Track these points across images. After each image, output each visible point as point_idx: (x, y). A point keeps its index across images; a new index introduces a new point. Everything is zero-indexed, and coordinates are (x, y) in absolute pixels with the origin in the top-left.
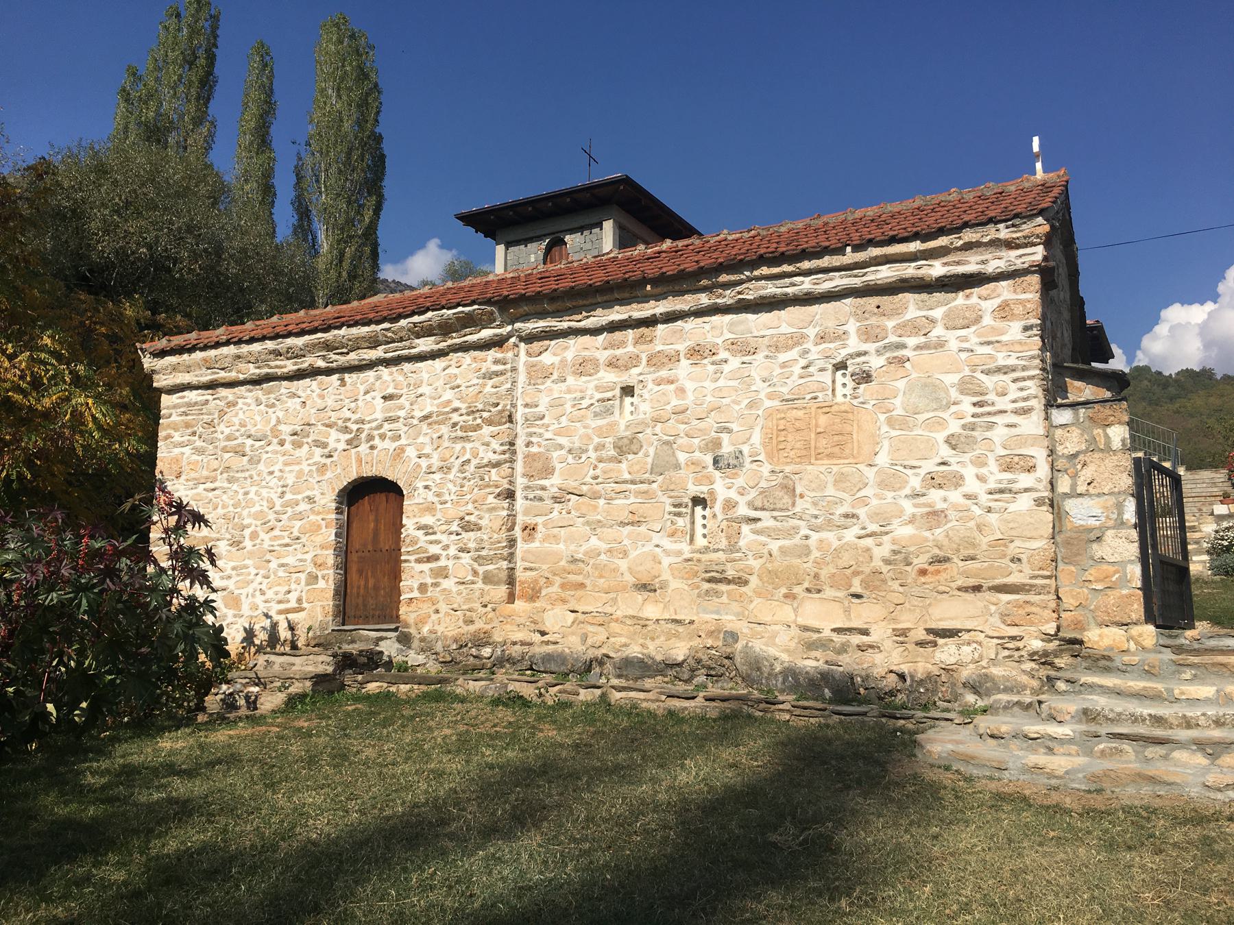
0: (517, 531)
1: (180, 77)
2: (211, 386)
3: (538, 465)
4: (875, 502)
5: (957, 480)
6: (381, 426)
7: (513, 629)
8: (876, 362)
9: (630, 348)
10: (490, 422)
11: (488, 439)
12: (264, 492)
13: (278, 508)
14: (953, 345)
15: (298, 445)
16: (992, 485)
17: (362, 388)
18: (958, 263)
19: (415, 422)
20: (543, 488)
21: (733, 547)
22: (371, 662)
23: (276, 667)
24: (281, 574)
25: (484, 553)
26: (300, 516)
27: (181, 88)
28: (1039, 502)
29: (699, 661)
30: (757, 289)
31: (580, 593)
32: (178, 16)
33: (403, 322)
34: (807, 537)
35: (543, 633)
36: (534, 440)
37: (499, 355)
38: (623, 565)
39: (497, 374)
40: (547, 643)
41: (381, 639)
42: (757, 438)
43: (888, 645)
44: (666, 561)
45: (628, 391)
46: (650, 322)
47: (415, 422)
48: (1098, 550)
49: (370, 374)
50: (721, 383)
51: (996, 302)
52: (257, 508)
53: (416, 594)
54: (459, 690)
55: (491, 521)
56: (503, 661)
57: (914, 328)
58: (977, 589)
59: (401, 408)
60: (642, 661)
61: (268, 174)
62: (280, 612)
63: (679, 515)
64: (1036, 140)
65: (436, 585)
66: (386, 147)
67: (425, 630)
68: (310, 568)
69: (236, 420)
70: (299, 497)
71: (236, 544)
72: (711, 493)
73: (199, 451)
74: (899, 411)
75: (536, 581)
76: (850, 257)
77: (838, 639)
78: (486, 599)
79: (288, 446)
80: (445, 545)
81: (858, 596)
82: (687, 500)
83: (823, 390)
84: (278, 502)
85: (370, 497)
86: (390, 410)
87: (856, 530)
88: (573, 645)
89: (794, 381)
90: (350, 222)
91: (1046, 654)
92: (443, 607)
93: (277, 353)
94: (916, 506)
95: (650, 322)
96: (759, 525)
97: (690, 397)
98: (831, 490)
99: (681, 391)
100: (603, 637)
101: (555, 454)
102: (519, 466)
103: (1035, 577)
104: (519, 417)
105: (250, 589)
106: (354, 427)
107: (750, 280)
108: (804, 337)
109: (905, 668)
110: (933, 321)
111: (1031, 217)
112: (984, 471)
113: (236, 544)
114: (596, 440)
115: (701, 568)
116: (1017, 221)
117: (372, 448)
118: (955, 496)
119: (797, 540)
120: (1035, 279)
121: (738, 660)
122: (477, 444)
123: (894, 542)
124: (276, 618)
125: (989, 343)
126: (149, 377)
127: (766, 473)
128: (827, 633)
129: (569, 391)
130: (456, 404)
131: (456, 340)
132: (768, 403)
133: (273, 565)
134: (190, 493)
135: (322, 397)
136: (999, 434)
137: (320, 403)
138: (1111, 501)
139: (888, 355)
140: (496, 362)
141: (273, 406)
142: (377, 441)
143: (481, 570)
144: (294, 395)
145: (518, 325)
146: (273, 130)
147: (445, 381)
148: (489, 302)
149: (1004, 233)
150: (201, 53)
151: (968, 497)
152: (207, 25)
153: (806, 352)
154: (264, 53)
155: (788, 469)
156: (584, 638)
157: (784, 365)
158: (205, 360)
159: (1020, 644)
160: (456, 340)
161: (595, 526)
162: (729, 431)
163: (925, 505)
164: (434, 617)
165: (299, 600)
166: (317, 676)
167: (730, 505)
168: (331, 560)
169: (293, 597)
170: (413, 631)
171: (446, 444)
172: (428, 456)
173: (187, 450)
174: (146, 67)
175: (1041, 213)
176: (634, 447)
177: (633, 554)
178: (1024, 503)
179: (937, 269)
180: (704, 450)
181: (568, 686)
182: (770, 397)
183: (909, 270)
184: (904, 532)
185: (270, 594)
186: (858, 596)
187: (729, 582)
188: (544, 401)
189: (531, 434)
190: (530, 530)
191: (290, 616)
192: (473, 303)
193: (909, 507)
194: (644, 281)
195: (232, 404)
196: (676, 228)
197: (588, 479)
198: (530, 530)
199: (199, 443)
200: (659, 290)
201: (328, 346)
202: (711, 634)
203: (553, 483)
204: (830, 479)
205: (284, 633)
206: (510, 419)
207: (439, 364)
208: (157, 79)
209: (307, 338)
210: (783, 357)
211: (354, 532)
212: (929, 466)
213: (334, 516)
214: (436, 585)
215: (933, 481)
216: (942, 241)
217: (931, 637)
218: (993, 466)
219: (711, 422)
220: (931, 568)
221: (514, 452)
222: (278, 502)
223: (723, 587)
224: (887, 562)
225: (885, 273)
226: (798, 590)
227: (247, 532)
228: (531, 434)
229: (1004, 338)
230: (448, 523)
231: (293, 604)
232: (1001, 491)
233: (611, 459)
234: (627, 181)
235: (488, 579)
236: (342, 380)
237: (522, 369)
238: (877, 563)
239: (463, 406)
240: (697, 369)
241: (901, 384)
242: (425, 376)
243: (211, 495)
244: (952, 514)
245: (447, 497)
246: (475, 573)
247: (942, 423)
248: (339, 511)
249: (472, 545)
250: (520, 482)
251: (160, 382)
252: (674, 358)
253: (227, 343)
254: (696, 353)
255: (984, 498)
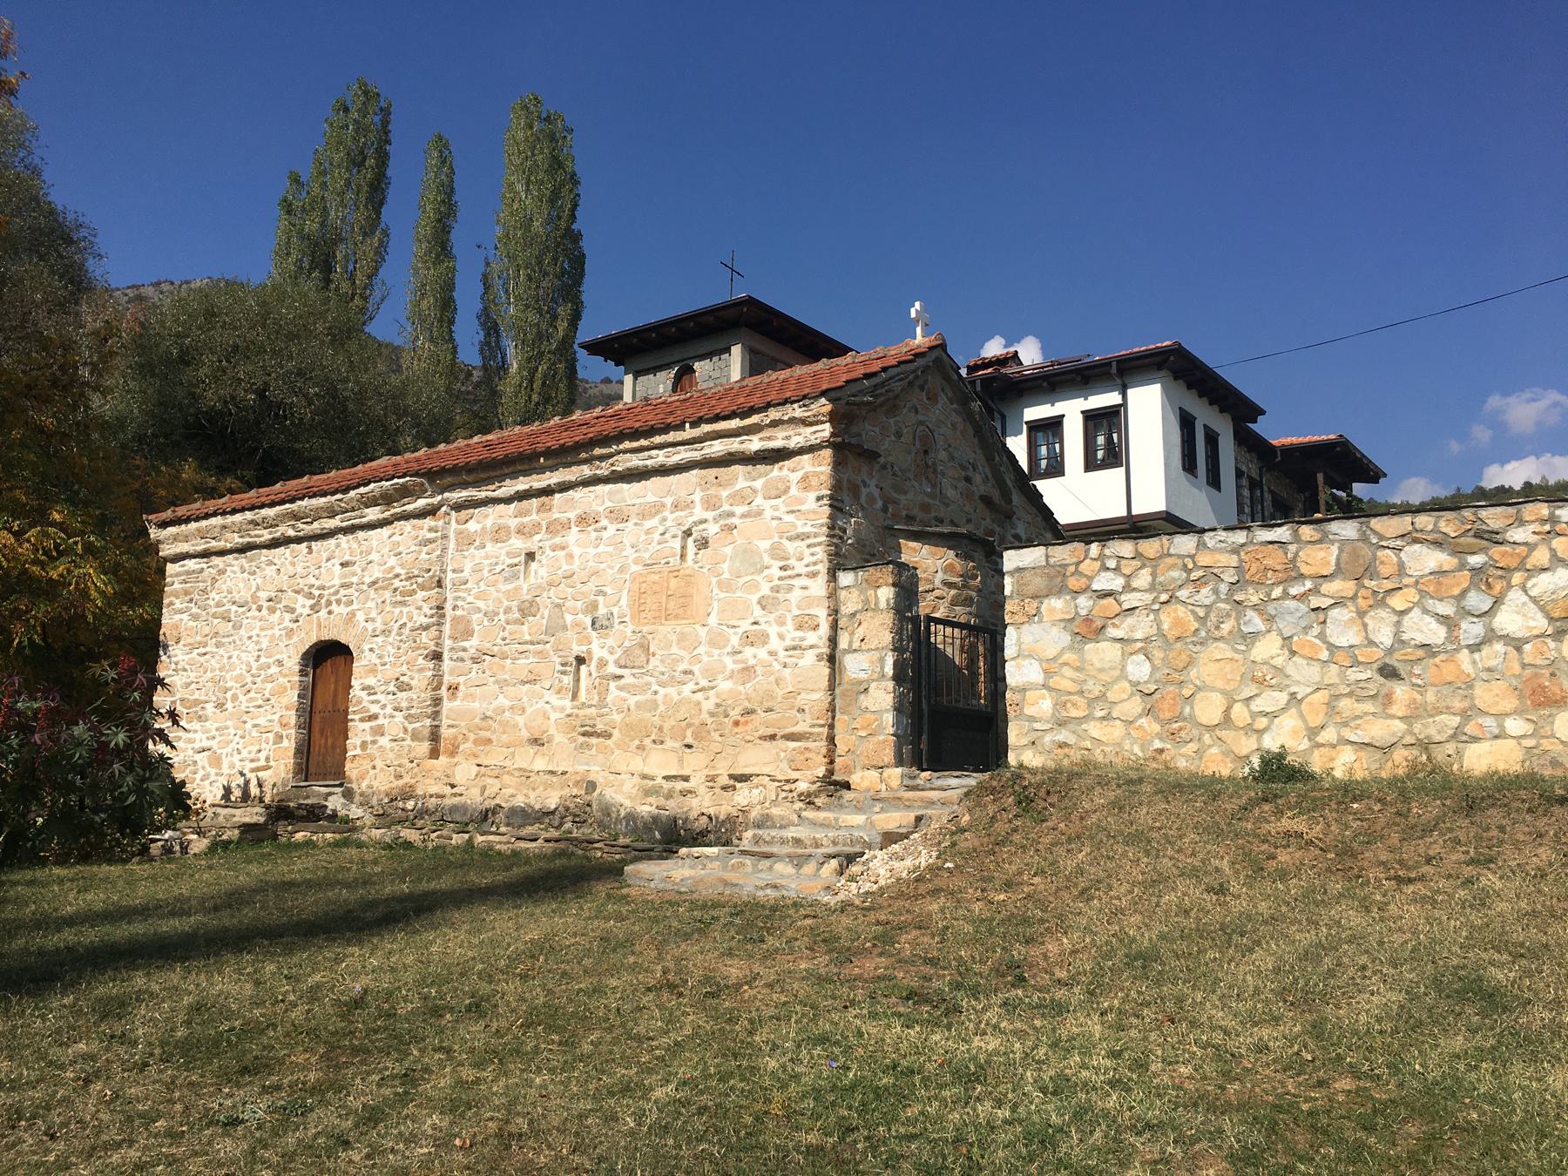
0: (444, 691)
1: (348, 183)
2: (206, 554)
3: (461, 627)
4: (705, 659)
5: (764, 638)
6: (337, 592)
7: (430, 786)
8: (712, 529)
9: (534, 516)
10: (423, 588)
11: (421, 603)
12: (243, 655)
13: (254, 671)
14: (768, 513)
15: (272, 611)
16: (788, 643)
17: (325, 556)
18: (769, 438)
19: (365, 587)
20: (464, 650)
21: (602, 704)
22: (314, 815)
23: (221, 819)
24: (254, 734)
25: (413, 711)
26: (270, 679)
27: (350, 195)
28: (819, 658)
29: (567, 809)
30: (624, 461)
31: (488, 748)
32: (346, 110)
33: (352, 493)
34: (656, 693)
35: (453, 786)
36: (459, 603)
37: (433, 523)
38: (521, 720)
39: (431, 541)
40: (455, 795)
41: (330, 794)
42: (624, 602)
43: (702, 790)
44: (553, 716)
45: (530, 556)
46: (547, 492)
47: (365, 587)
48: (864, 701)
49: (332, 542)
50: (601, 548)
51: (799, 474)
52: (238, 671)
53: (358, 751)
54: (364, 838)
55: (420, 681)
56: (423, 813)
57: (742, 498)
58: (773, 737)
59: (354, 574)
60: (523, 810)
61: (448, 287)
62: (253, 770)
63: (564, 673)
64: (917, 305)
65: (374, 742)
66: (586, 245)
67: (364, 785)
68: (277, 728)
69: (224, 587)
70: (271, 660)
71: (220, 706)
72: (589, 652)
73: (195, 618)
74: (726, 575)
75: (455, 738)
76: (689, 433)
77: (667, 785)
78: (412, 756)
79: (265, 612)
80: (382, 704)
81: (689, 746)
82: (572, 659)
83: (674, 555)
84: (254, 665)
85: (328, 658)
86: (345, 576)
87: (691, 686)
88: (473, 798)
89: (654, 547)
90: (540, 336)
91: (809, 795)
92: (379, 764)
93: (255, 523)
94: (735, 662)
95: (547, 492)
96: (623, 681)
97: (577, 562)
98: (674, 650)
99: (570, 556)
100: (496, 789)
101: (475, 617)
102: (447, 629)
103: (813, 726)
104: (448, 583)
105: (229, 749)
106: (317, 593)
107: (619, 453)
108: (663, 505)
109: (712, 811)
110: (755, 491)
111: (816, 398)
112: (783, 629)
113: (220, 706)
114: (506, 603)
115: (579, 723)
116: (807, 402)
117: (330, 613)
118: (762, 653)
119: (648, 696)
120: (827, 453)
121: (594, 806)
122: (412, 608)
123: (718, 696)
124: (249, 775)
125: (793, 512)
126: (154, 548)
127: (629, 634)
128: (659, 780)
129: (487, 557)
130: (398, 570)
131: (397, 509)
132: (634, 568)
133: (248, 726)
134: (186, 658)
135: (293, 564)
136: (796, 595)
137: (291, 571)
138: (877, 655)
139: (722, 522)
140: (430, 530)
141: (254, 573)
142: (334, 607)
143: (410, 727)
144: (271, 563)
145: (446, 495)
146: (453, 236)
147: (390, 549)
148: (416, 474)
149: (798, 411)
150: (370, 152)
151: (771, 653)
152: (377, 119)
153: (664, 519)
154: (442, 144)
155: (645, 629)
156: (483, 789)
157: (648, 532)
158: (198, 530)
159: (793, 786)
160: (397, 509)
161: (503, 684)
162: (605, 594)
163: (742, 662)
164: (372, 772)
165: (267, 759)
166: (245, 825)
167: (602, 663)
168: (293, 721)
169: (262, 755)
170: (354, 786)
171: (388, 608)
172: (373, 620)
173: (185, 617)
174: (307, 172)
175: (823, 394)
176: (533, 610)
177: (529, 711)
178: (810, 657)
179: (754, 444)
180: (585, 612)
181: (445, 832)
182: (636, 562)
183: (734, 445)
184: (725, 686)
185: (245, 754)
186: (689, 746)
187: (599, 735)
188: (468, 566)
189: (456, 598)
190: (453, 689)
191: (260, 774)
192: (404, 476)
193: (729, 663)
194: (535, 456)
195: (222, 572)
196: (842, 350)
197: (499, 641)
198: (453, 689)
199: (195, 610)
200: (550, 462)
201: (296, 516)
202: (577, 783)
203: (472, 644)
204: (674, 638)
205: (254, 791)
206: (440, 584)
207: (385, 532)
208: (324, 185)
209: (278, 508)
210: (648, 524)
211: (318, 693)
212: (745, 625)
213: (297, 678)
214: (374, 742)
215: (748, 639)
216: (755, 419)
217: (732, 782)
218: (790, 625)
219: (591, 586)
220: (742, 720)
221: (444, 616)
222: (254, 665)
223: (594, 740)
224: (712, 714)
225: (717, 448)
226: (647, 741)
227: (229, 694)
228: (456, 598)
229: (803, 508)
230: (387, 683)
231: (262, 763)
232: (794, 648)
233: (516, 622)
234: (750, 301)
235: (415, 736)
236: (309, 548)
237: (452, 536)
238: (705, 716)
239: (403, 572)
240: (583, 536)
241: (728, 550)
242: (375, 543)
243: (202, 659)
244: (759, 669)
245: (386, 659)
246: (406, 730)
247: (756, 586)
248: (303, 673)
249: (404, 704)
250: (448, 643)
251: (166, 551)
252: (566, 526)
253: (215, 514)
254: (583, 520)
255: (782, 654)
